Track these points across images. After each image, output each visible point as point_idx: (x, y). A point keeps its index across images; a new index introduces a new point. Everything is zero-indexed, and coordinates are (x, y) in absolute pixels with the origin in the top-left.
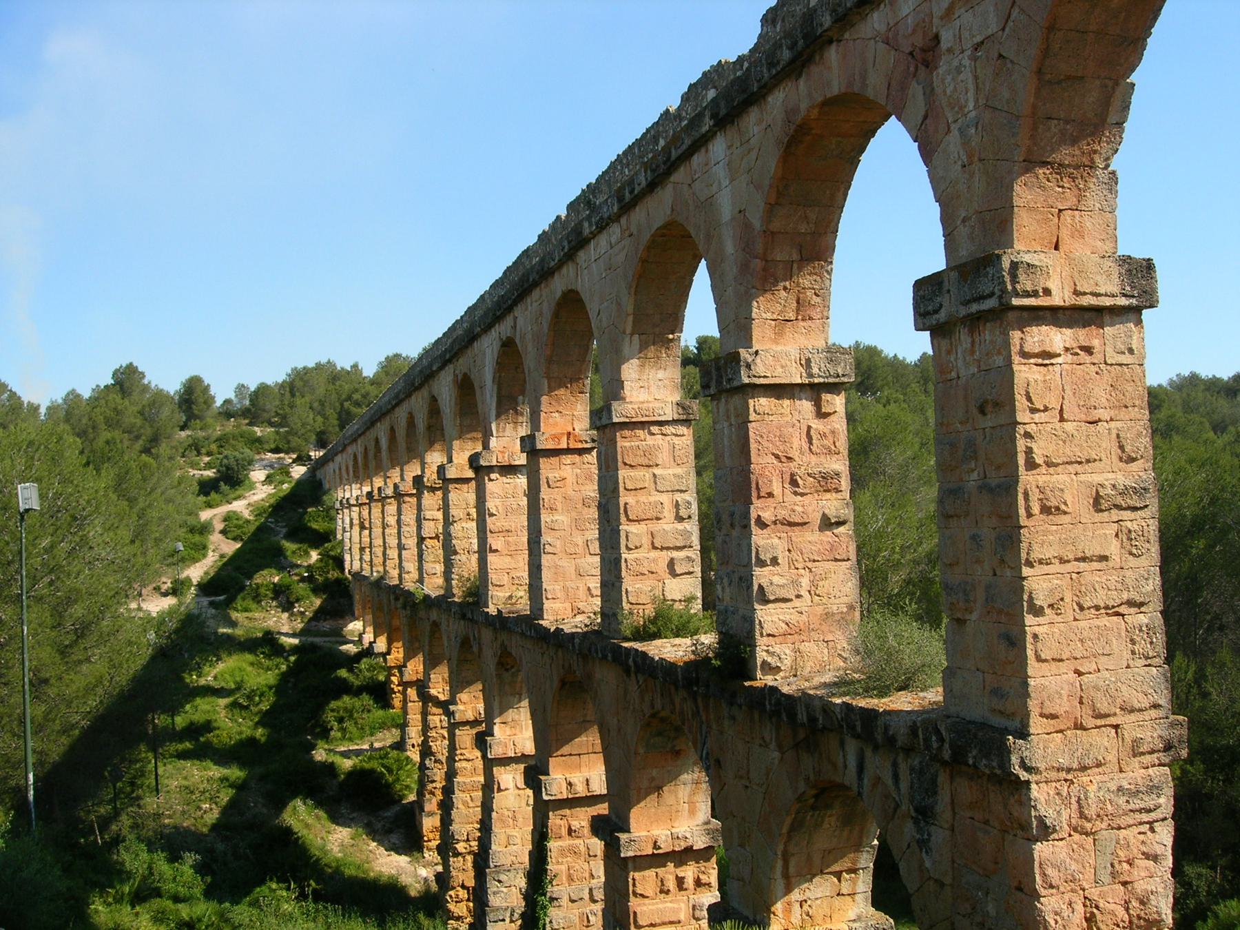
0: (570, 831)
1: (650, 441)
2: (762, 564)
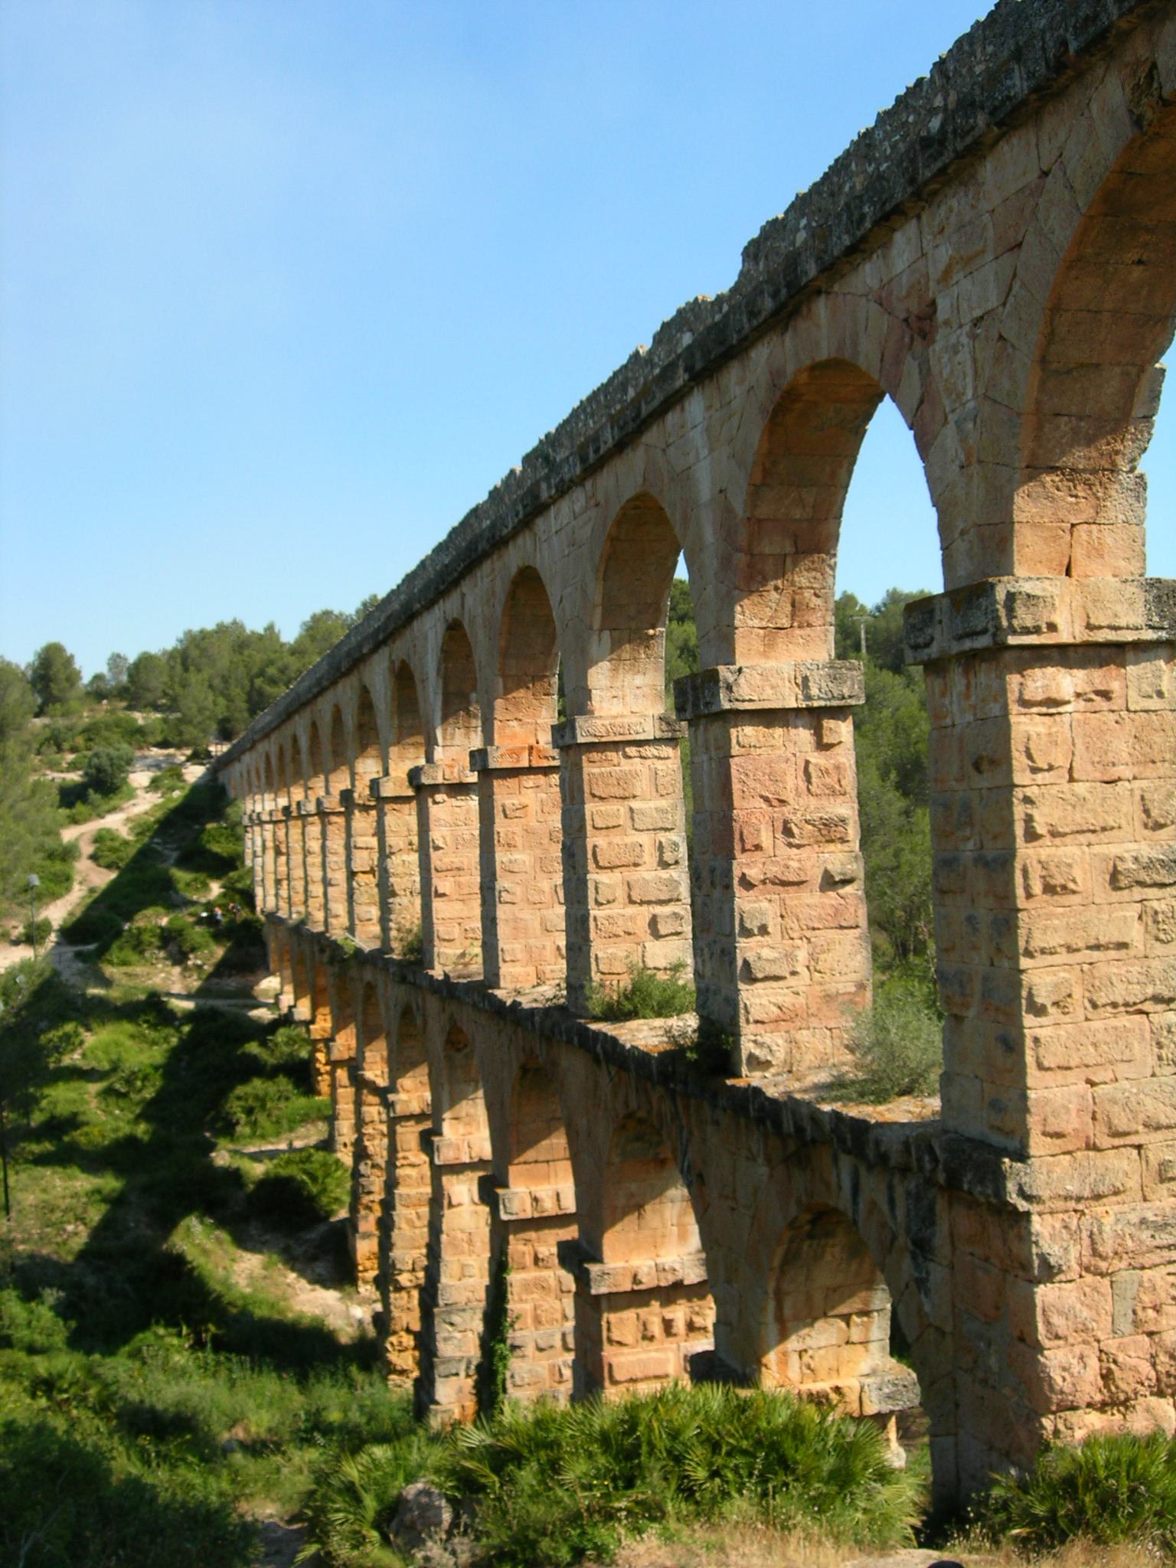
0: (537, 1260)
1: (626, 765)
2: (747, 933)
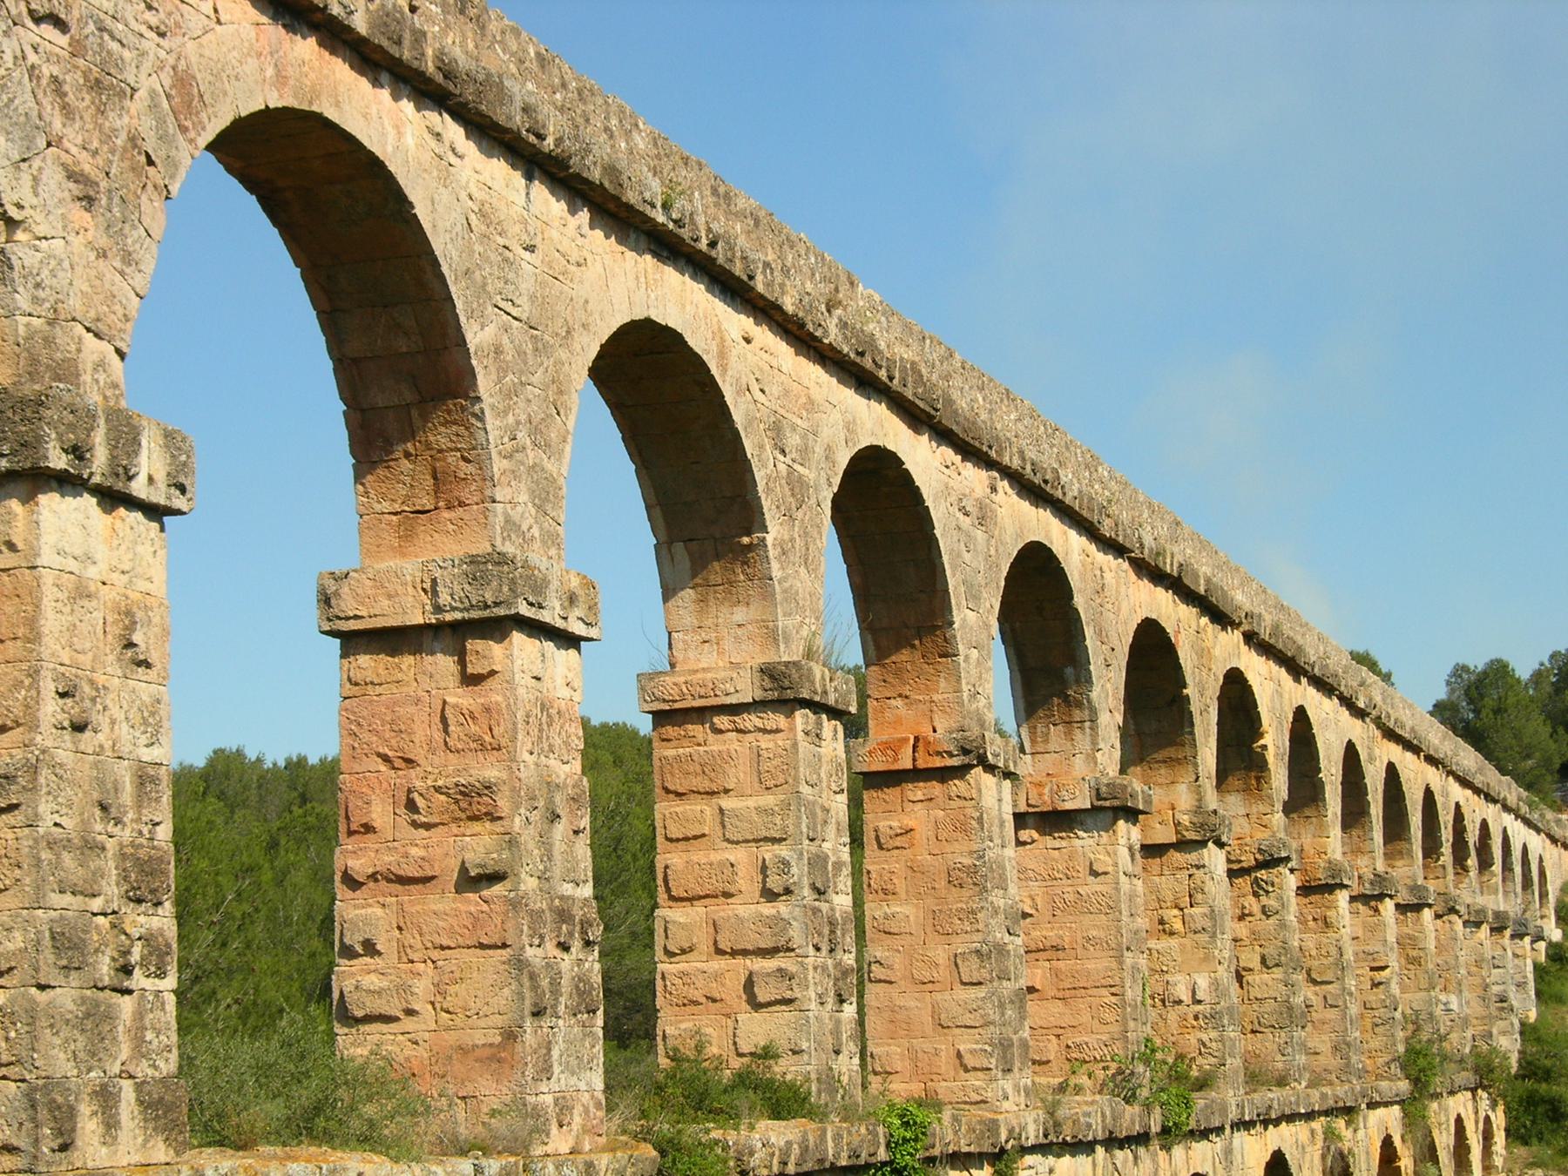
1: (715, 745)
2: (348, 952)
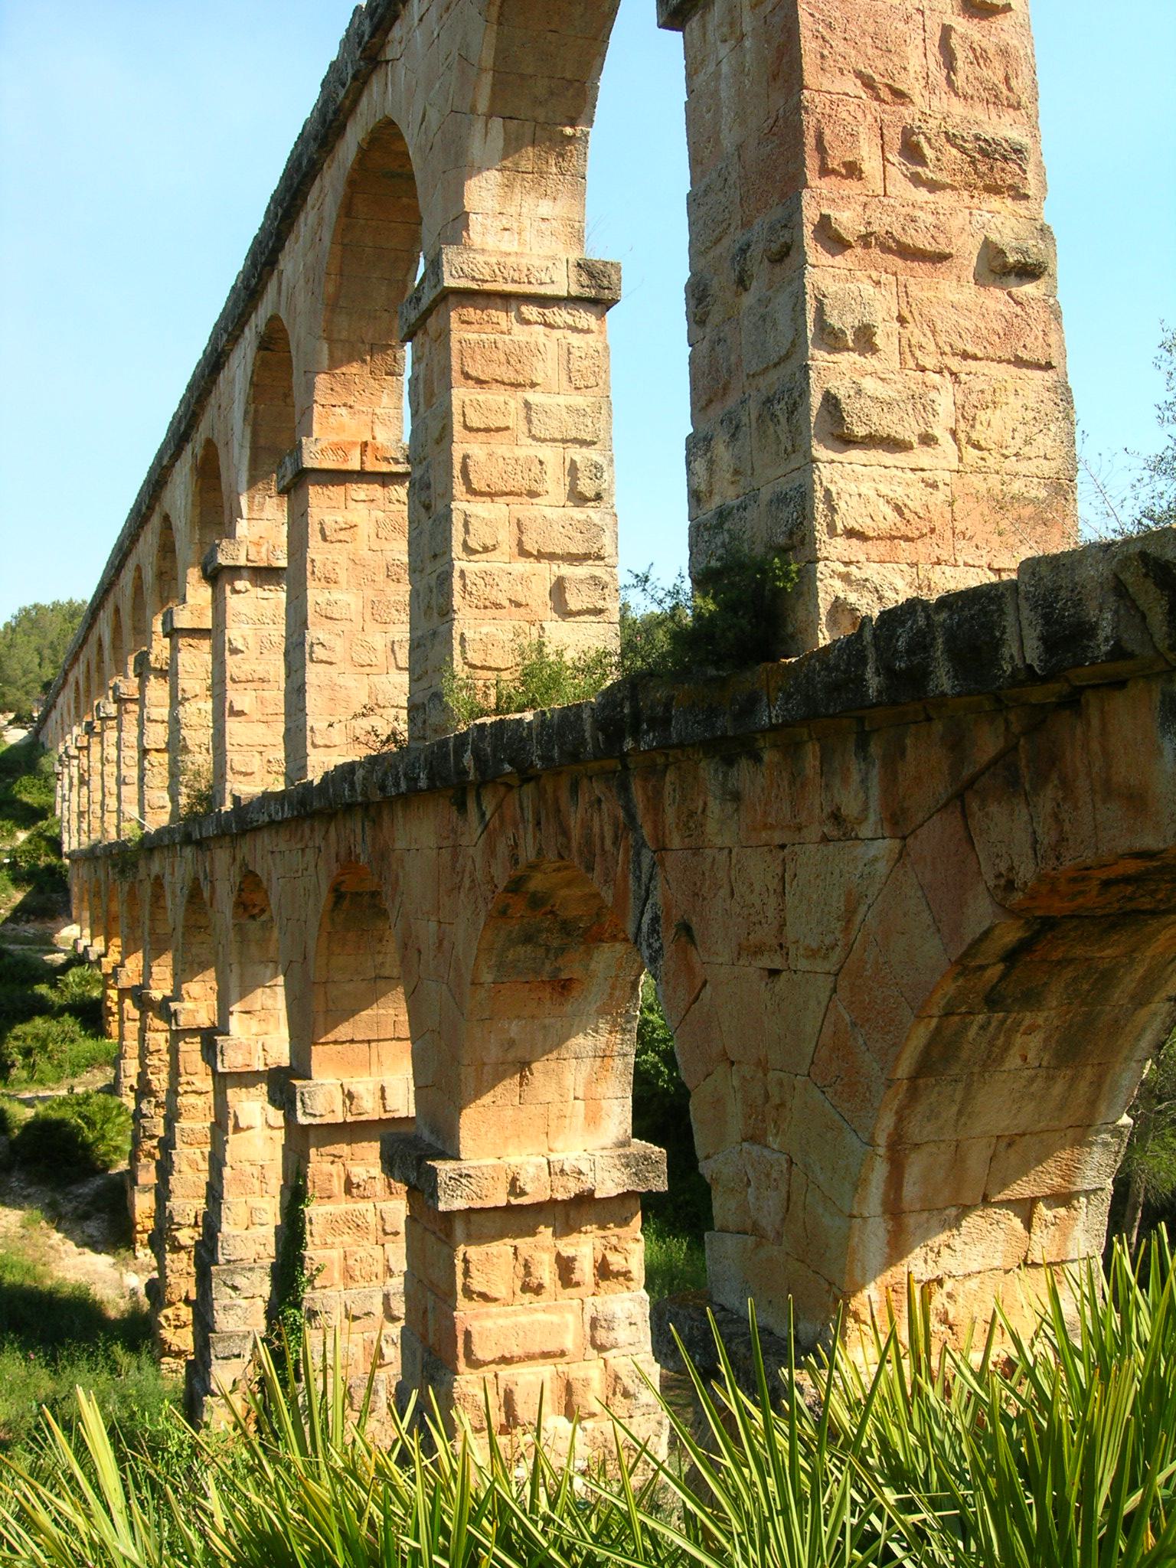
0: (349, 1186)
1: (520, 333)
2: (832, 339)
